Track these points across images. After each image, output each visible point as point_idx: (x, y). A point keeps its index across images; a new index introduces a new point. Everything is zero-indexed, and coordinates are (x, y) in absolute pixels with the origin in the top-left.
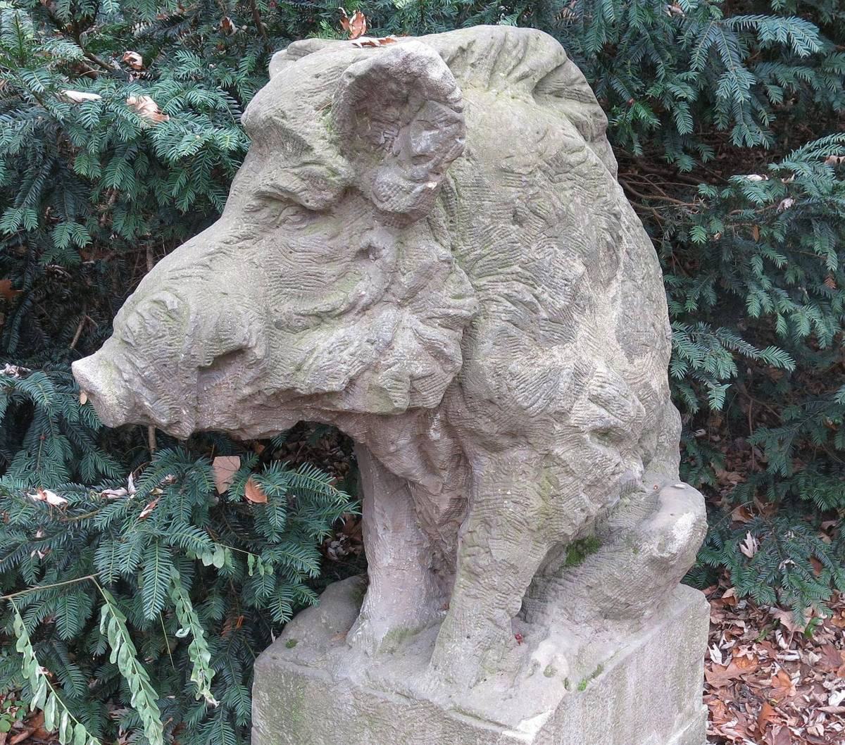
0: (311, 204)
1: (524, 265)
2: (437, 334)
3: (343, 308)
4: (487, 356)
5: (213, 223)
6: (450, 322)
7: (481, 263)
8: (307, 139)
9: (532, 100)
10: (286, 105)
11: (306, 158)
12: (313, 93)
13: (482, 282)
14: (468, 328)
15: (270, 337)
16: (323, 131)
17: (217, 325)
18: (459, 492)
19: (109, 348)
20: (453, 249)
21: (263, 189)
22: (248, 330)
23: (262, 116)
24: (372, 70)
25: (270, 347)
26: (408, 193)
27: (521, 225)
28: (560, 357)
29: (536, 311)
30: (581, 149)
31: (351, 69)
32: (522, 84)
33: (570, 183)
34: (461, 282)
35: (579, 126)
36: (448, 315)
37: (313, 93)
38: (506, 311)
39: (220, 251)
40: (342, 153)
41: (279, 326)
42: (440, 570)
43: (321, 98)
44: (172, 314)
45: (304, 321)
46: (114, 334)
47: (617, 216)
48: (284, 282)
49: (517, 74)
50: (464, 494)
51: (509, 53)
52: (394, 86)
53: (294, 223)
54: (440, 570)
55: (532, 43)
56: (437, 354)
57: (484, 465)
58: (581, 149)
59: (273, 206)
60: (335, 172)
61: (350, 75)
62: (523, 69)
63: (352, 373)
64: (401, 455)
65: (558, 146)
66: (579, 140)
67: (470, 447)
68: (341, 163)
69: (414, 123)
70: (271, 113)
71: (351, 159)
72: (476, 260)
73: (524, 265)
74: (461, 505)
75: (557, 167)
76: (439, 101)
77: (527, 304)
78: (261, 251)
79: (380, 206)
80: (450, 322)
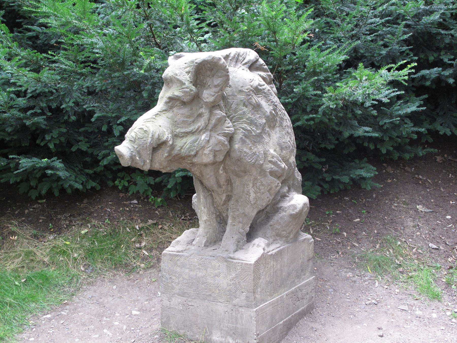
0: (185, 100)
1: (247, 119)
2: (222, 138)
3: (194, 131)
4: (237, 146)
5: (147, 111)
6: (225, 135)
7: (235, 118)
8: (184, 81)
9: (248, 71)
10: (177, 72)
11: (184, 87)
12: (185, 68)
13: (235, 124)
14: (231, 138)
15: (173, 139)
16: (189, 79)
17: (159, 136)
18: (228, 193)
19: (124, 143)
20: (226, 114)
21: (170, 96)
22: (167, 136)
23: (170, 75)
24: (203, 61)
25: (173, 142)
26: (213, 96)
27: (246, 107)
28: (260, 149)
29: (251, 133)
30: (264, 85)
31: (197, 61)
32: (245, 66)
33: (261, 95)
34: (229, 123)
35: (264, 79)
36: (225, 133)
37: (185, 68)
38: (242, 132)
39: (158, 114)
40: (194, 85)
41: (176, 136)
42: (222, 221)
43: (187, 70)
44: (146, 131)
45: (183, 135)
46: (126, 139)
47: (276, 106)
48: (175, 124)
49: (243, 63)
50: (230, 194)
51: (241, 56)
52: (209, 66)
53: (179, 106)
54: (222, 221)
55: (248, 53)
56: (223, 144)
57: (237, 182)
58: (264, 85)
59: (174, 101)
60: (191, 90)
61: (196, 63)
62: (245, 61)
63: (197, 149)
64: (210, 178)
65: (257, 84)
66: (264, 83)
67: (233, 177)
68: (193, 88)
69: (215, 76)
70: (172, 74)
71: (196, 87)
72: (233, 117)
73: (247, 119)
74: (229, 198)
75: (257, 90)
76: (222, 70)
77: (248, 130)
78: (170, 114)
79: (205, 101)
80: (225, 135)
